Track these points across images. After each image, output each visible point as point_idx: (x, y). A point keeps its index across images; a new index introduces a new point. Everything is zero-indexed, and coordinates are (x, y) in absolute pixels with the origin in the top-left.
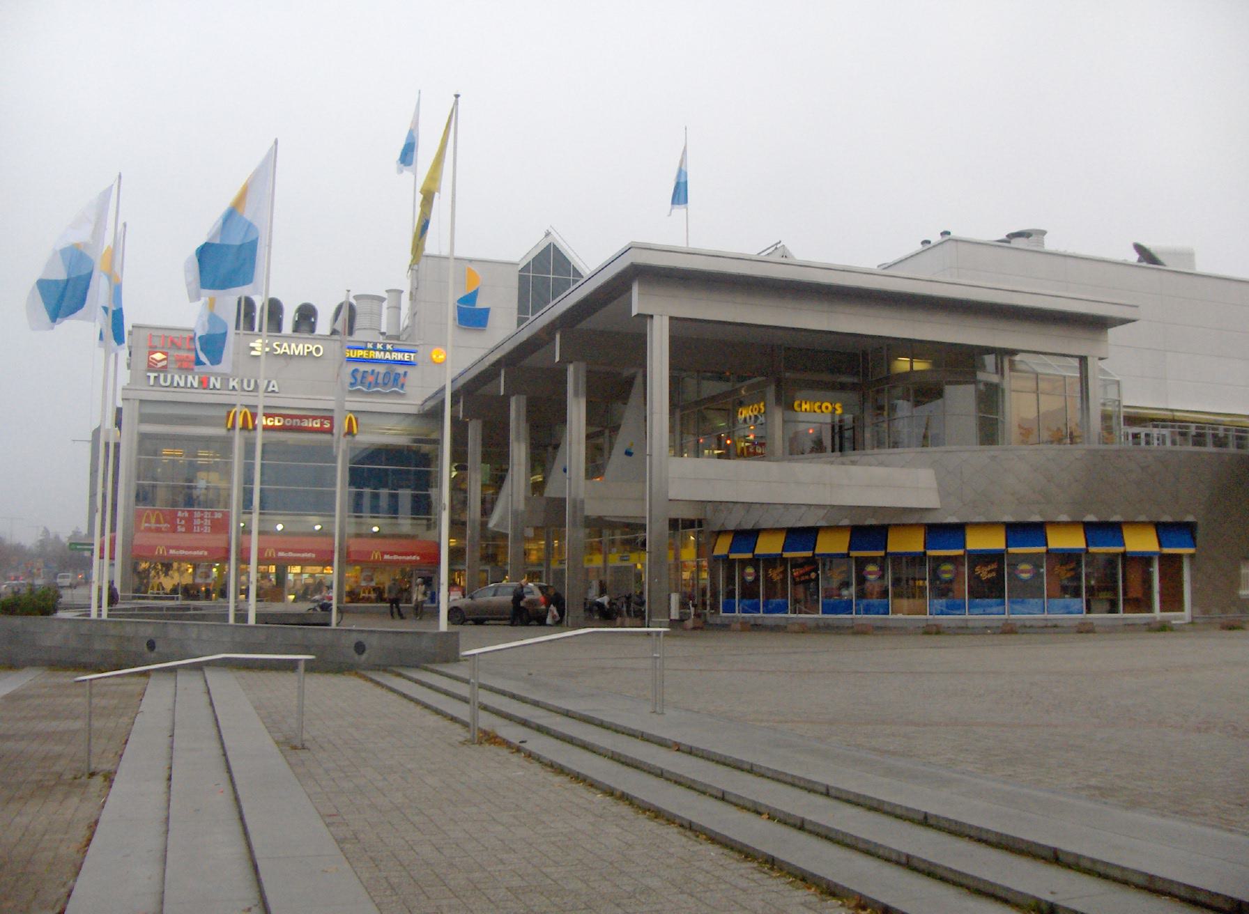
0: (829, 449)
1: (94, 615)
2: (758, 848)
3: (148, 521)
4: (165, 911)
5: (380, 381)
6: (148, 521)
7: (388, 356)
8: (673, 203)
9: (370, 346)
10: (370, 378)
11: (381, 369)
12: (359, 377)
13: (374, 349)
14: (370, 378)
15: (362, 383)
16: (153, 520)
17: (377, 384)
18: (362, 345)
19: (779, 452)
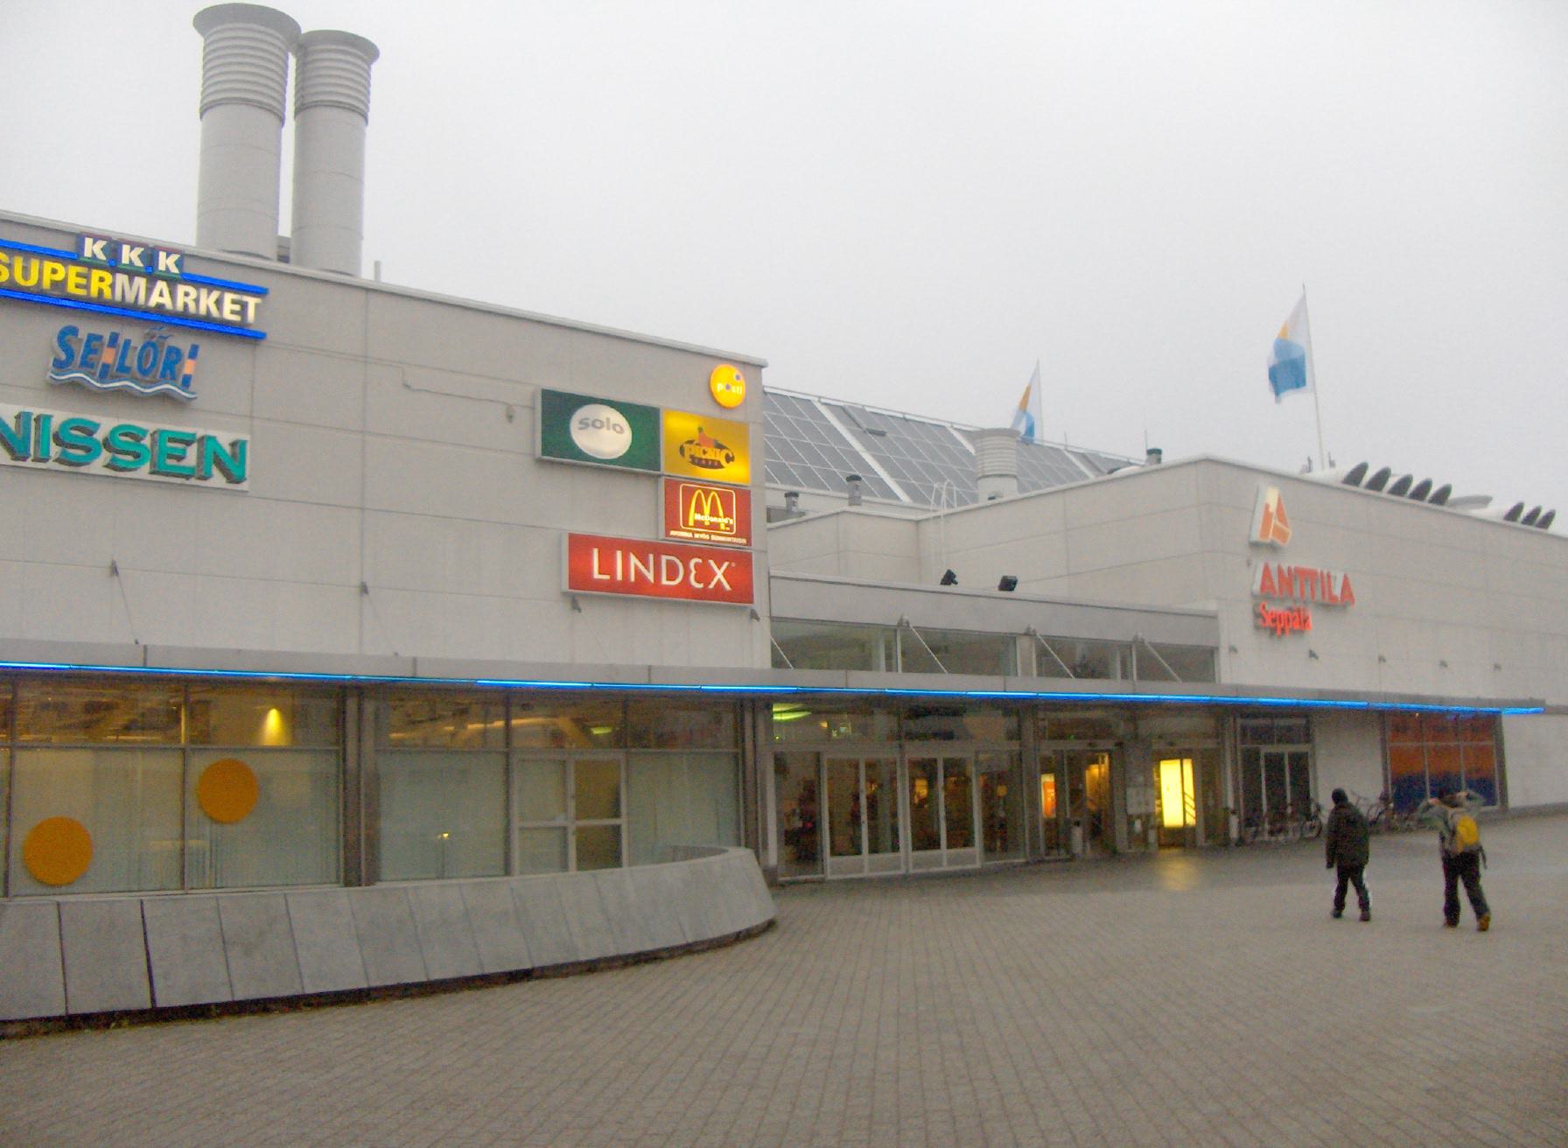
0: (1119, 675)
1: (619, 577)
2: (1110, 637)
3: (699, 510)
4: (5, 1043)
5: (132, 361)
6: (699, 510)
7: (160, 296)
8: (1277, 393)
9: (92, 249)
10: (108, 356)
11: (134, 335)
12: (80, 350)
13: (113, 265)
14: (108, 356)
15: (86, 364)
16: (707, 509)
17: (123, 370)
18: (63, 245)
19: (1024, 645)
